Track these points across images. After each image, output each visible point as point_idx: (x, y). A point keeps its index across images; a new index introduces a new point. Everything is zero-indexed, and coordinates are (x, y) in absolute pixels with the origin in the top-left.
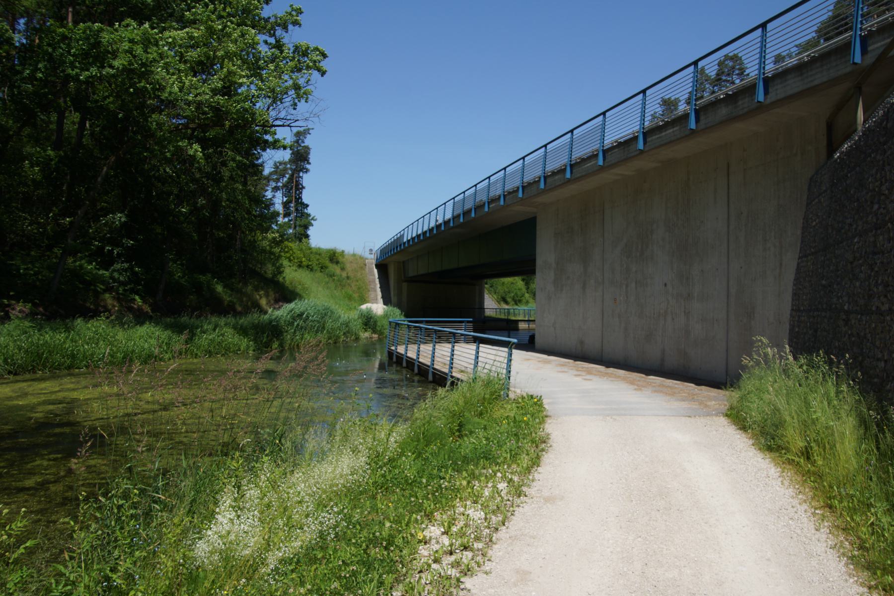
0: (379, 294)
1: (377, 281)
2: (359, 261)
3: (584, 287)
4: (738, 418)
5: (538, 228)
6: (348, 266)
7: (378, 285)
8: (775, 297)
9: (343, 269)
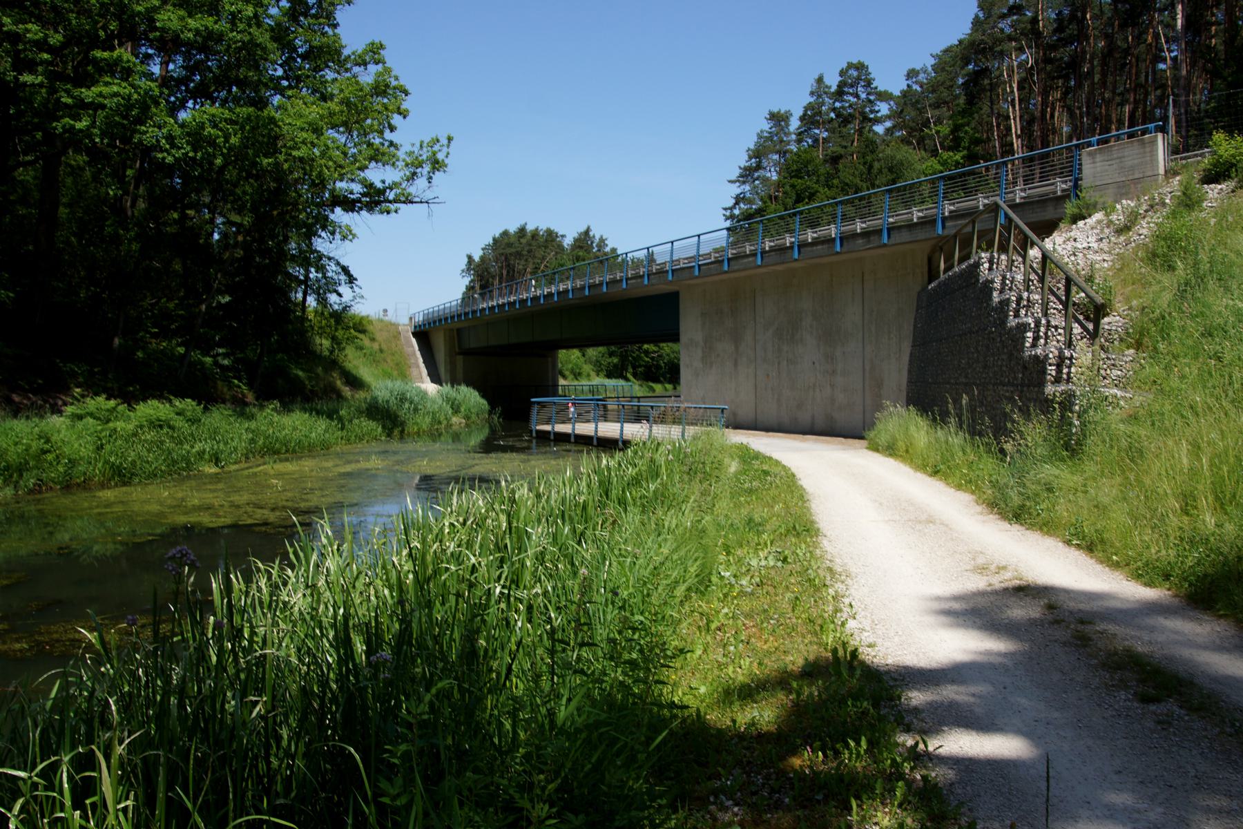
0: (424, 371)
1: (418, 354)
2: (393, 330)
3: (736, 364)
4: (875, 448)
5: (681, 306)
6: (378, 336)
7: (421, 360)
8: (896, 372)
9: (373, 340)
